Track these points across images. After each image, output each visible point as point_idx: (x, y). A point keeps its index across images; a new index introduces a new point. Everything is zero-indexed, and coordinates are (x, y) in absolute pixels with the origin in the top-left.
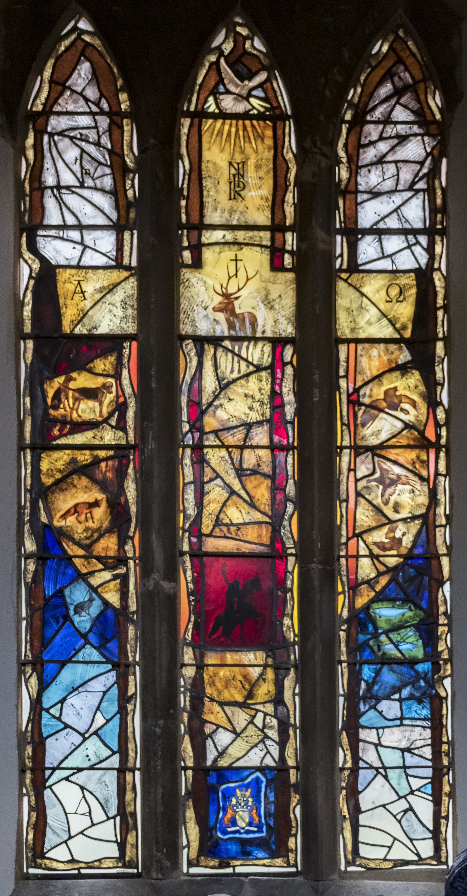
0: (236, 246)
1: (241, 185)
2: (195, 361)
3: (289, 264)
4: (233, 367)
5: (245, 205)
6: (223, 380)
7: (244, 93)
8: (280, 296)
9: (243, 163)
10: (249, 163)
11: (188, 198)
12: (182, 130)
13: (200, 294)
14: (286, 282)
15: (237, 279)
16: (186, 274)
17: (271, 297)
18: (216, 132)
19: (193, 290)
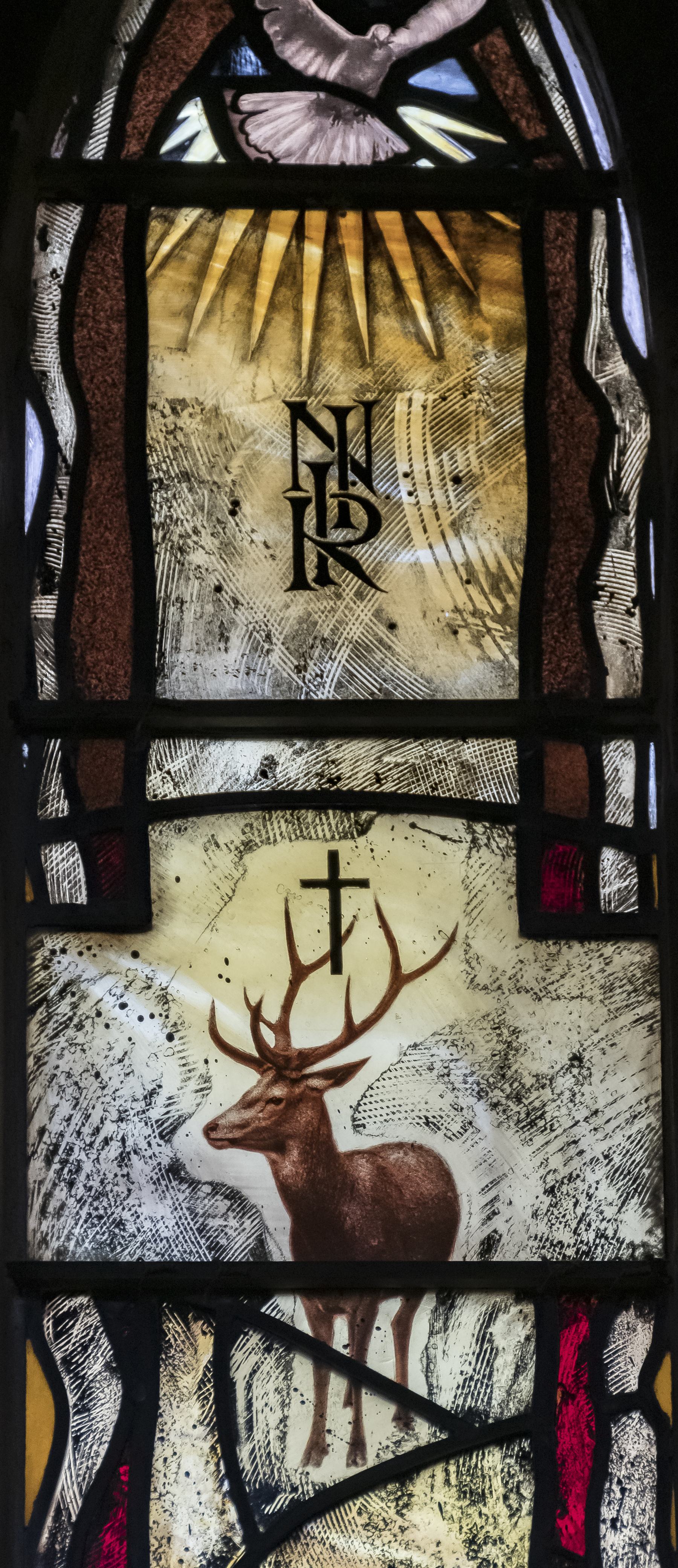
0: (333, 817)
1: (359, 515)
2: (107, 1407)
3: (623, 896)
4: (319, 1430)
5: (378, 614)
6: (271, 1500)
7: (367, 76)
8: (577, 1059)
9: (369, 406)
10: (400, 407)
11: (67, 588)
12: (39, 259)
13: (139, 1057)
14: (608, 989)
15: (341, 979)
16: (65, 959)
17: (527, 1066)
18: (218, 266)
19: (97, 1039)
